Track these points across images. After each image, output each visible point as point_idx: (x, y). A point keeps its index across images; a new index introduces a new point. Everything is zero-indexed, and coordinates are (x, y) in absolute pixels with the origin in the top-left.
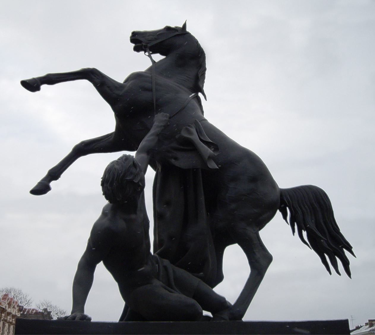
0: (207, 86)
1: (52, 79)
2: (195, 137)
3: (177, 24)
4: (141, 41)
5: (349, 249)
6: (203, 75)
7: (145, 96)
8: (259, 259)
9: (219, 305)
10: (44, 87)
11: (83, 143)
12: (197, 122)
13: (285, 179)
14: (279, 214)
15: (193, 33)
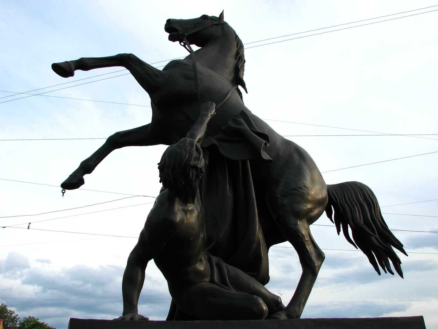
0: (247, 76)
1: (86, 64)
4: (176, 30)
5: (400, 247)
6: (243, 66)
8: (311, 261)
10: (78, 72)
13: (332, 168)
15: (230, 24)
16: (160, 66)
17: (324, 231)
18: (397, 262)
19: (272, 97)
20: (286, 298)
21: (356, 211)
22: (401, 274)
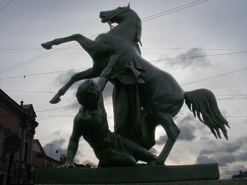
0: (142, 39)
1: (57, 42)
2: (132, 67)
3: (124, 5)
4: (106, 17)
5: (226, 123)
7: (106, 47)
9: (150, 158)
10: (54, 46)
12: (134, 59)
17: (184, 115)
18: (225, 132)
19: (154, 51)
21: (204, 104)
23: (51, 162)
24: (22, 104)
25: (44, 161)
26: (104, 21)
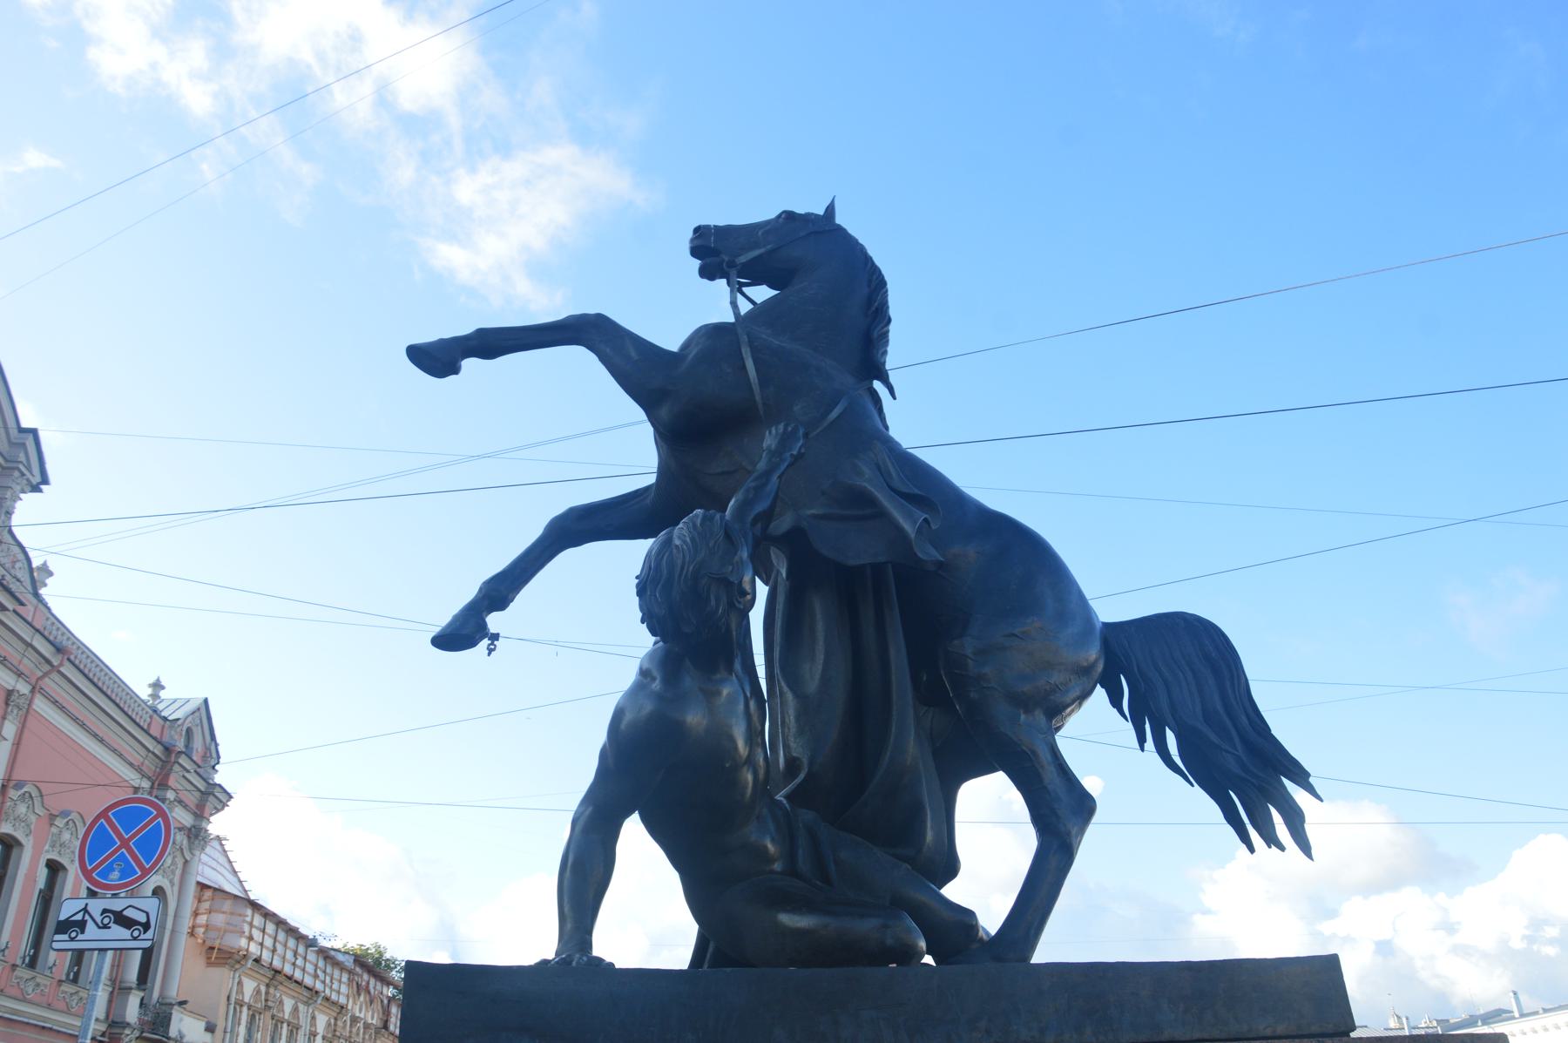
0: (893, 359)
4: (717, 252)
5: (1301, 776)
8: (1060, 812)
10: (470, 365)
11: (572, 511)
13: (1117, 586)
14: (1100, 693)
15: (853, 230)
16: (671, 341)
17: (1097, 739)
20: (991, 919)
22: (1305, 847)
23: (272, 990)
24: (155, 696)
25: (240, 983)
26: (707, 273)
